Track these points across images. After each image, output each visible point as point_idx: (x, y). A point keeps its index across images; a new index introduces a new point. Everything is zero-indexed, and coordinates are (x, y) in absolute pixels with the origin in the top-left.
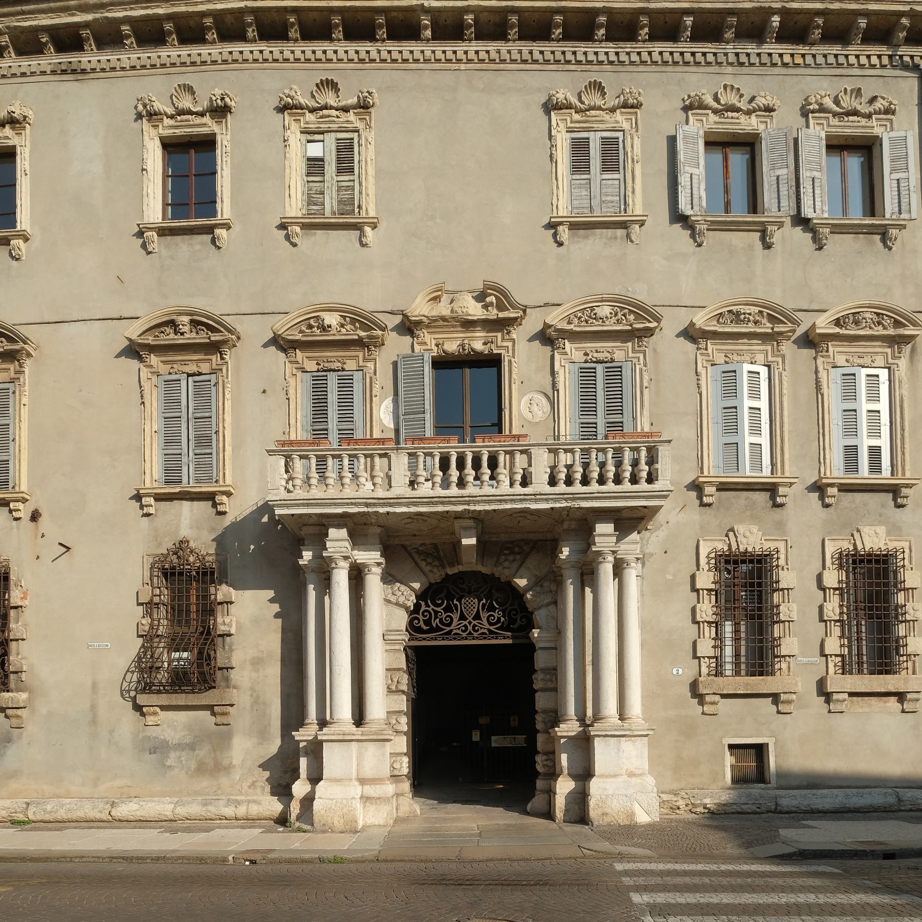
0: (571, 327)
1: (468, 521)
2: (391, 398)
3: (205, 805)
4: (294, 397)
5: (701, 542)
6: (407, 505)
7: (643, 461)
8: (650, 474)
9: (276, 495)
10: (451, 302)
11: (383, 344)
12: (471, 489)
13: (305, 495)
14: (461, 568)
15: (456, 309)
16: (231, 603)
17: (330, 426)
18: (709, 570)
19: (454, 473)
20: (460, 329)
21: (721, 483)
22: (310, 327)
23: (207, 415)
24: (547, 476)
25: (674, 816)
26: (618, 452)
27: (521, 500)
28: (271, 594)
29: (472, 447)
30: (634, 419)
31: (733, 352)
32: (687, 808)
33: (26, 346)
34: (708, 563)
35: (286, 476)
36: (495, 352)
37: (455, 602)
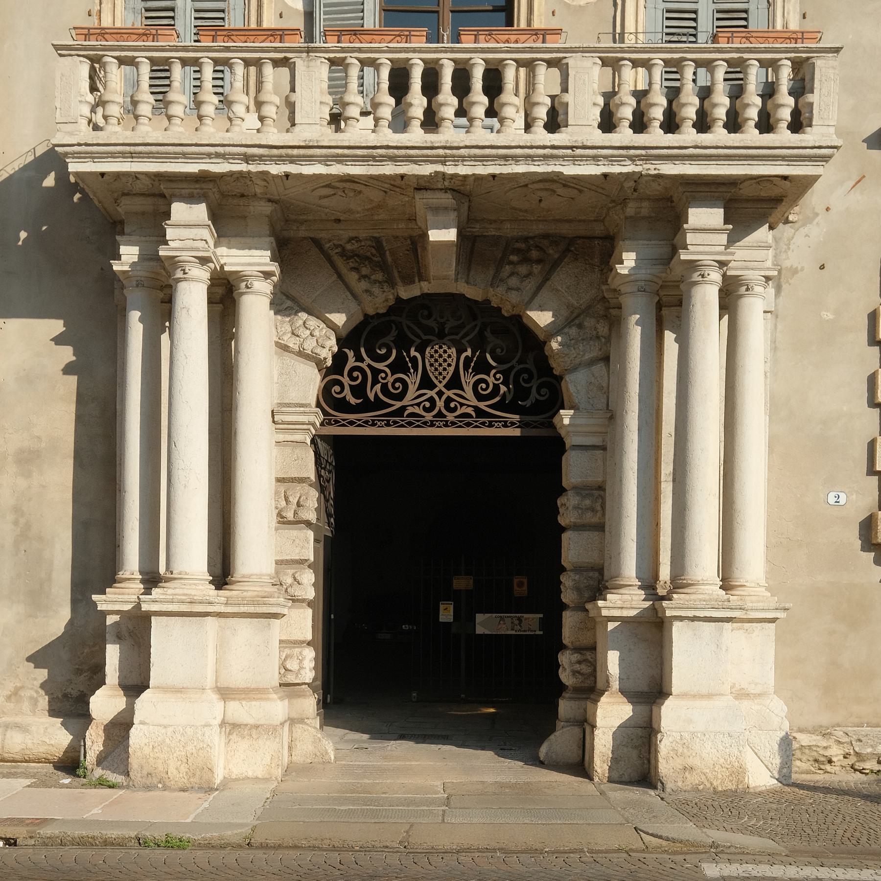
37: (413, 353)
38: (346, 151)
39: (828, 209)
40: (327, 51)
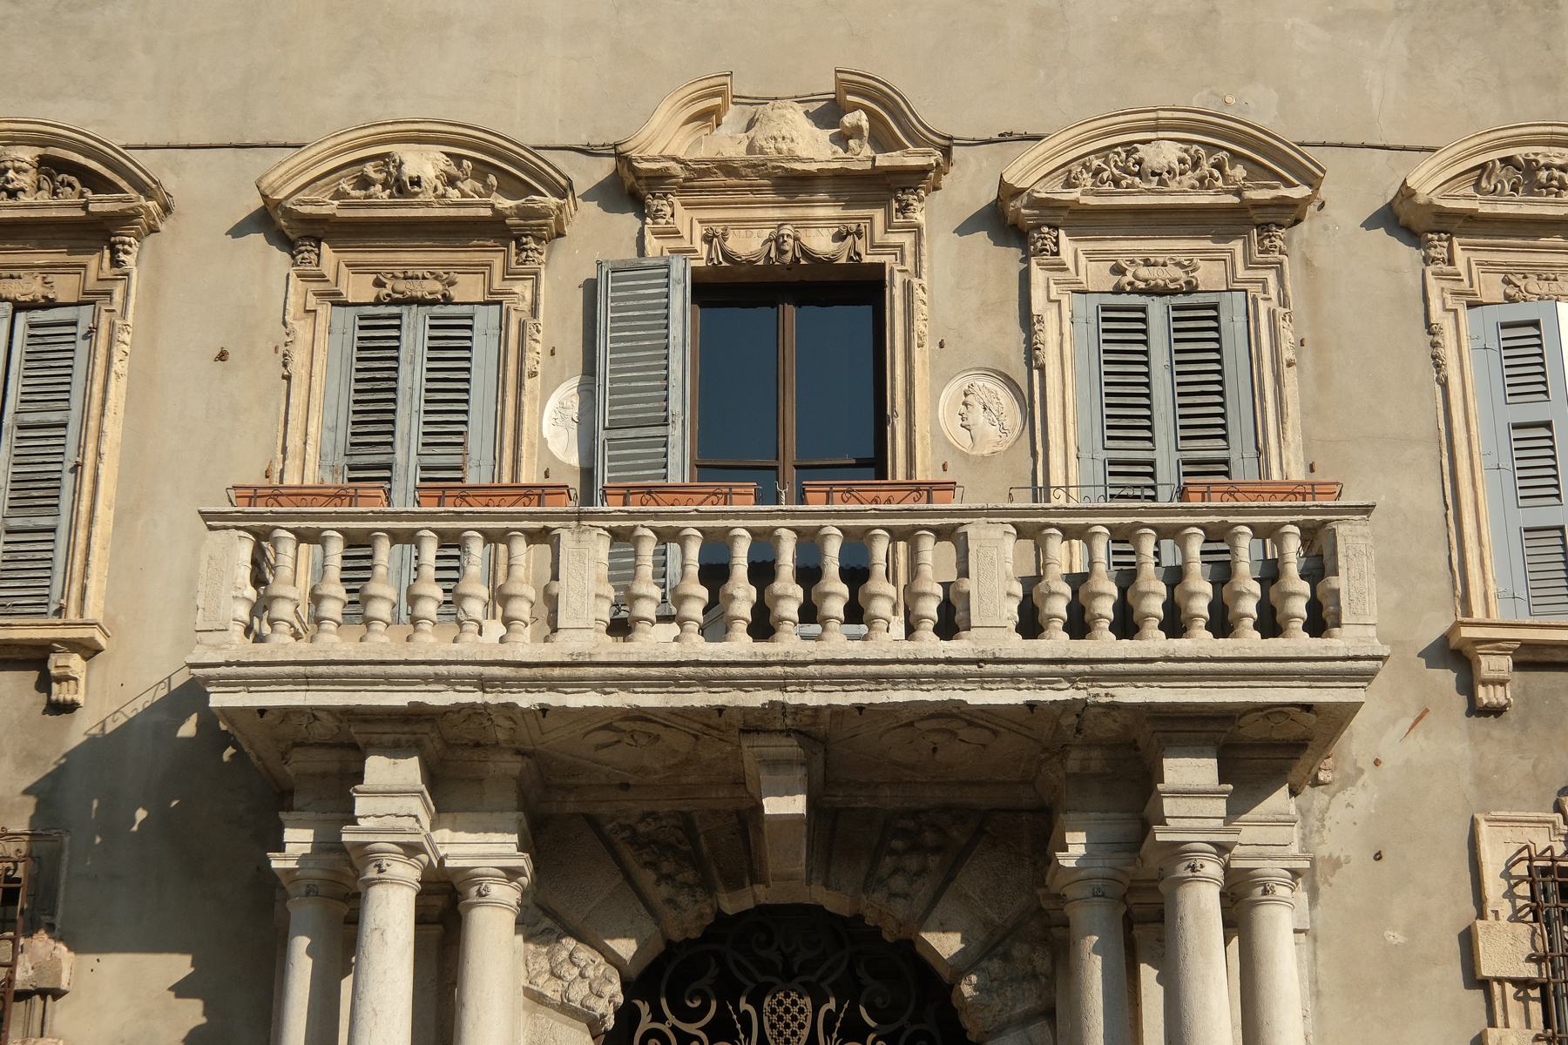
0: (1075, 194)
1: (784, 741)
2: (576, 381)
4: (304, 372)
5: (1483, 828)
6: (602, 685)
7: (1293, 566)
8: (1314, 606)
9: (217, 647)
10: (750, 126)
11: (560, 234)
12: (790, 642)
13: (303, 650)
14: (762, 894)
15: (760, 142)
16: (57, 994)
17: (400, 456)
18: (1515, 918)
19: (742, 594)
20: (770, 197)
21: (1527, 645)
22: (364, 183)
23: (55, 417)
24: (1014, 606)
26: (1215, 534)
27: (938, 677)
28: (180, 966)
29: (793, 515)
30: (1261, 451)
31: (1525, 270)
34: (1510, 895)
35: (251, 593)
36: (867, 259)
37: (744, 1005)
38: (634, 671)
40: (606, 516)
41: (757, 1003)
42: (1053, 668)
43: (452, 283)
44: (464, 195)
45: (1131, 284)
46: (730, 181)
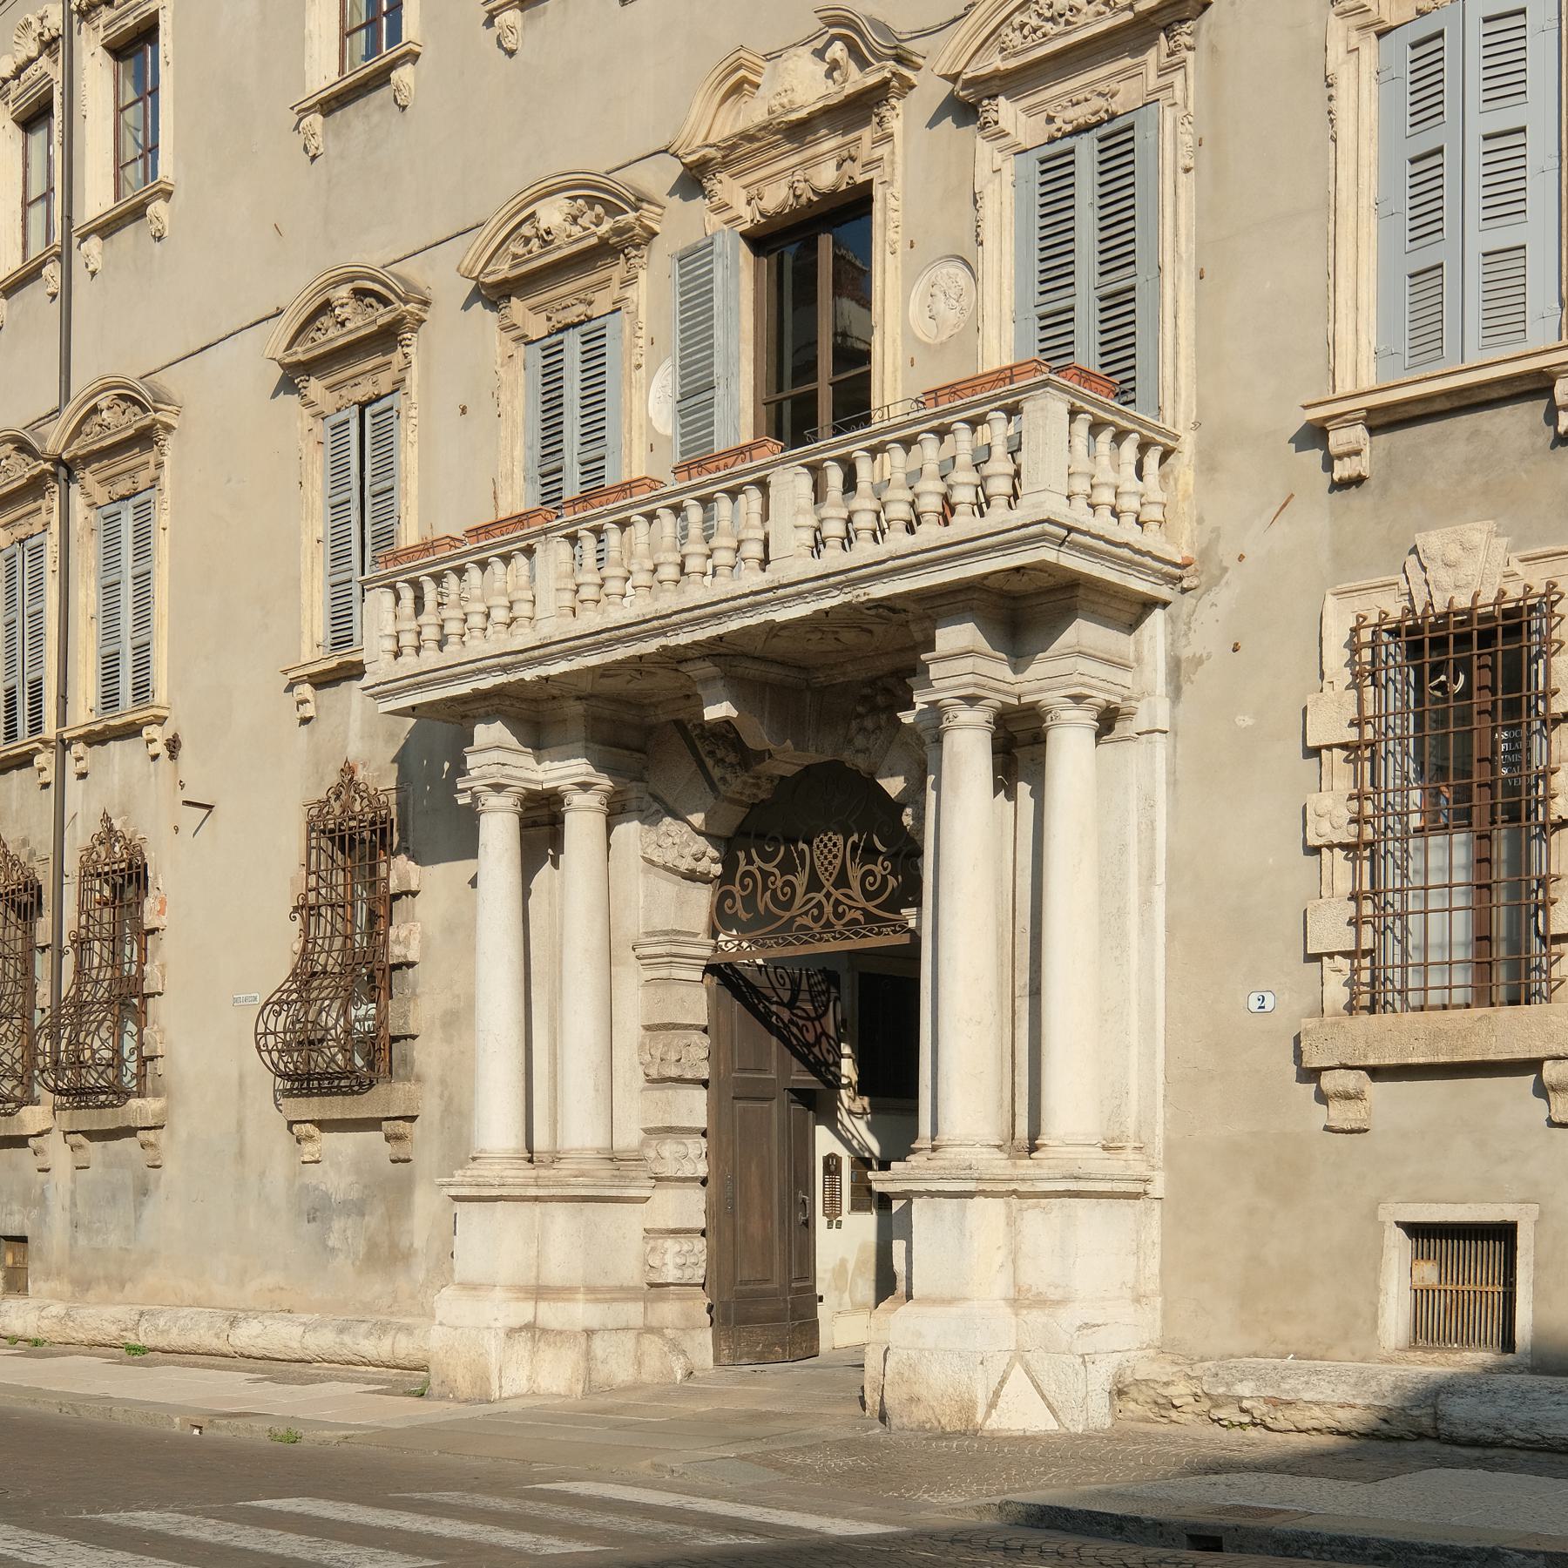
3: (341, 1331)
20: (788, 147)
21: (1369, 410)
25: (1163, 1428)
32: (1200, 1408)
33: (158, 416)
37: (801, 845)
38: (577, 643)
39: (1241, 558)
40: (559, 528)
41: (810, 843)
42: (821, 583)
43: (590, 303)
44: (585, 229)
45: (1059, 130)
46: (757, 145)
